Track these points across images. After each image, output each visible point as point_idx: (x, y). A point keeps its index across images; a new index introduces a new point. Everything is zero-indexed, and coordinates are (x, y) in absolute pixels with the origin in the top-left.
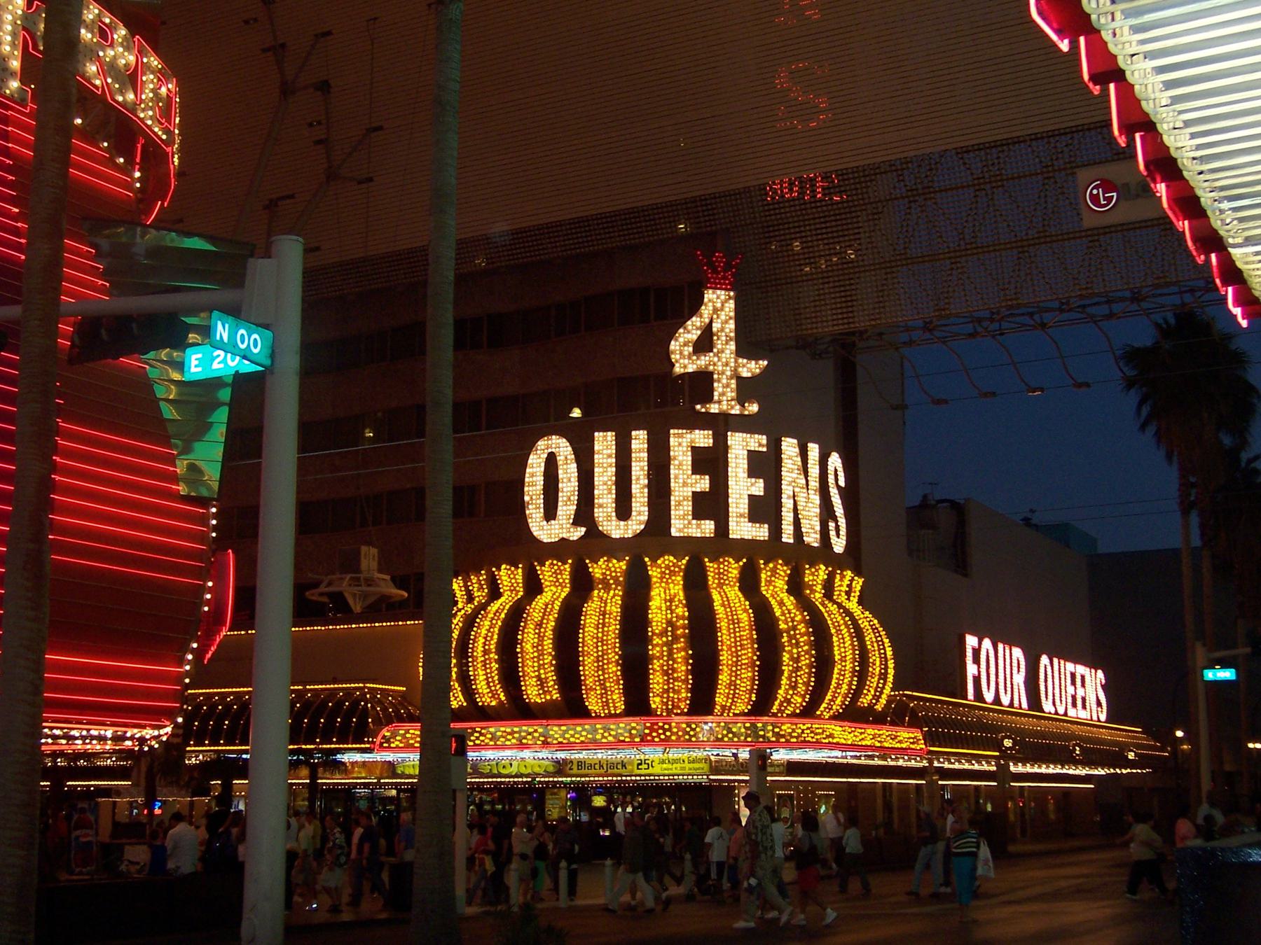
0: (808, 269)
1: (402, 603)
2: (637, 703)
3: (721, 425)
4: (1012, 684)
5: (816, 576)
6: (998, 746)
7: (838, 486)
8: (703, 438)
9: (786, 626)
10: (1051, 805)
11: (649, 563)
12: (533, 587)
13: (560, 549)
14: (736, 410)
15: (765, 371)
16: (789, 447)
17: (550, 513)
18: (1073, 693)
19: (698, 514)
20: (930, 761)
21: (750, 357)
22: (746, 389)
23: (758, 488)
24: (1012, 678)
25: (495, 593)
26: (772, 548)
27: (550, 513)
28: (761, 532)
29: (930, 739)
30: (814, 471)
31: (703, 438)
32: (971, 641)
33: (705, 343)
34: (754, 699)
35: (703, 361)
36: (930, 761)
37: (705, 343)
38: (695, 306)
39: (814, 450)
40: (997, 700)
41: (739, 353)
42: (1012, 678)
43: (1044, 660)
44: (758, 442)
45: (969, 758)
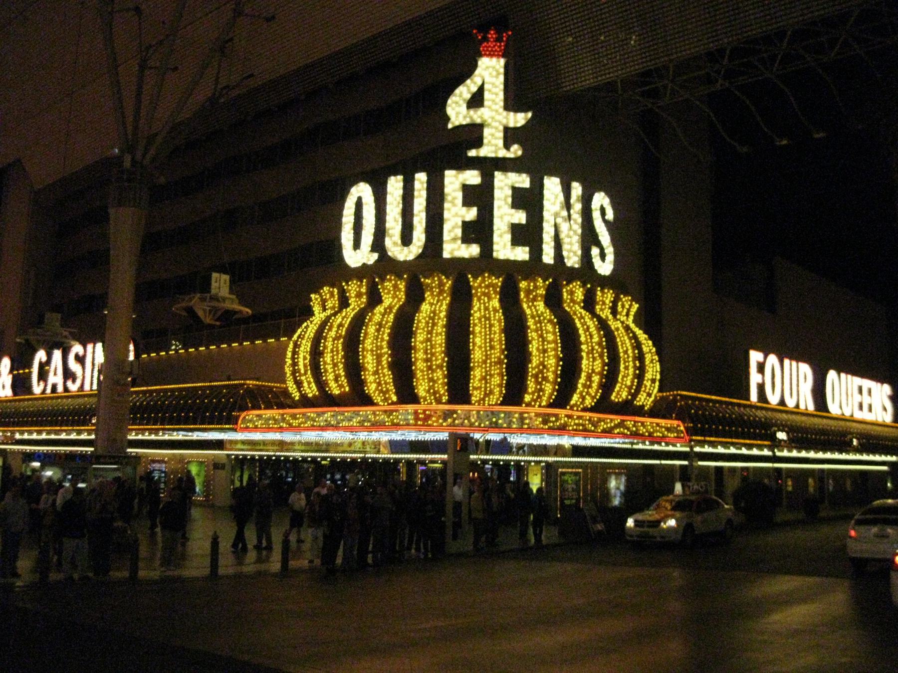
0: (570, 39)
1: (246, 320)
2: (407, 394)
3: (488, 167)
4: (798, 391)
5: (575, 292)
6: (773, 438)
7: (606, 222)
8: (473, 177)
9: (535, 327)
10: (848, 483)
11: (471, 279)
12: (374, 299)
13: (363, 272)
14: (502, 153)
15: (529, 122)
16: (552, 186)
17: (357, 245)
18: (760, 381)
19: (466, 239)
20: (691, 448)
21: (517, 110)
22: (510, 136)
23: (520, 217)
24: (798, 386)
25: (344, 302)
26: (534, 267)
27: (357, 245)
28: (522, 254)
29: (690, 432)
30: (577, 207)
31: (473, 177)
32: (755, 356)
33: (476, 101)
34: (504, 392)
35: (477, 116)
36: (691, 448)
37: (476, 101)
38: (469, 70)
39: (577, 189)
40: (782, 402)
41: (508, 107)
42: (798, 386)
43: (832, 375)
44: (523, 181)
45: (750, 447)
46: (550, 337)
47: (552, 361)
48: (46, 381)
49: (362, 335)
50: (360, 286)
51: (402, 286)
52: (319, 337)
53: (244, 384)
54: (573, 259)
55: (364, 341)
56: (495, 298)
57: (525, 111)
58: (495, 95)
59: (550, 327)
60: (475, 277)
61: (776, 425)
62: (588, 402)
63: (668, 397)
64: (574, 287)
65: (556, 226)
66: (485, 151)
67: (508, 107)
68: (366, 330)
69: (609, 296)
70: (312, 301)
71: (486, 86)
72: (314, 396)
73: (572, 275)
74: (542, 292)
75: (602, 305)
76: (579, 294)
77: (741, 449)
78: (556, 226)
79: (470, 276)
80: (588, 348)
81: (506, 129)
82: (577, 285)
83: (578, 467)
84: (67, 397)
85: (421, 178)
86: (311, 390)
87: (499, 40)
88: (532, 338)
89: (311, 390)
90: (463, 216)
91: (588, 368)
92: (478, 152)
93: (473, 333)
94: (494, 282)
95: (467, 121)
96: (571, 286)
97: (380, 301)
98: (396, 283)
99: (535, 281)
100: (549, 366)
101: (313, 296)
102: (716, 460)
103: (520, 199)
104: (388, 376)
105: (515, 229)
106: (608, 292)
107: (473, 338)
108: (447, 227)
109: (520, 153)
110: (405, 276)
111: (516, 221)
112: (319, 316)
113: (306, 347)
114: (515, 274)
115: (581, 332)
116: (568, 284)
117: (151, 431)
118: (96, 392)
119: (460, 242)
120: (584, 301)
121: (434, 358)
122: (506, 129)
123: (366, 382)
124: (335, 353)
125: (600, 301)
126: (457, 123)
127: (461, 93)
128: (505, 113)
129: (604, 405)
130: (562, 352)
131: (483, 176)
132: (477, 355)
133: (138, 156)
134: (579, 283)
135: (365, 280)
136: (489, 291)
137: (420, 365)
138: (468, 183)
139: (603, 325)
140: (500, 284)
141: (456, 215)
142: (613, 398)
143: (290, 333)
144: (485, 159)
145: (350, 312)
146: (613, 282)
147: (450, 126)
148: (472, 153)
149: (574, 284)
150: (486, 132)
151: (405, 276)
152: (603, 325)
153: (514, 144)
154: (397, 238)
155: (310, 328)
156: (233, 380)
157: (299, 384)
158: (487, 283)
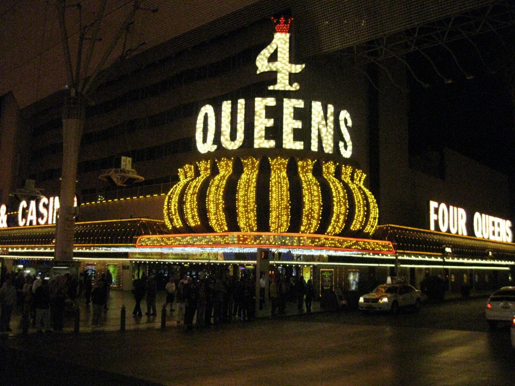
0: (327, 22)
1: (141, 184)
2: (233, 226)
3: (280, 96)
4: (458, 225)
5: (330, 168)
6: (443, 251)
7: (347, 127)
8: (271, 102)
9: (307, 188)
10: (487, 277)
11: (270, 160)
12: (215, 171)
13: (208, 156)
14: (288, 88)
15: (303, 70)
16: (317, 107)
17: (205, 141)
18: (436, 219)
19: (268, 137)
20: (397, 257)
21: (296, 63)
22: (293, 78)
23: (298, 124)
24: (458, 221)
25: (197, 173)
26: (306, 153)
27: (205, 141)
28: (299, 146)
29: (396, 248)
30: (331, 119)
31: (271, 102)
32: (433, 204)
33: (273, 58)
34: (289, 225)
35: (274, 66)
36: (397, 257)
37: (273, 58)
38: (269, 40)
39: (331, 108)
40: (449, 231)
41: (291, 61)
42: (458, 221)
43: (477, 215)
44: (300, 104)
45: (430, 256)
46: (316, 193)
47: (317, 207)
48: (26, 219)
49: (208, 192)
50: (207, 164)
51: (231, 164)
52: (183, 193)
53: (140, 220)
54: (328, 149)
55: (209, 195)
56: (284, 171)
57: (301, 63)
58: (284, 54)
59: (315, 188)
60: (273, 159)
61: (445, 244)
62: (337, 230)
63: (383, 228)
64: (329, 164)
65: (319, 130)
66: (278, 87)
67: (291, 61)
68: (210, 189)
69: (349, 170)
70: (179, 172)
71: (279, 50)
72: (180, 227)
73: (328, 158)
74: (311, 167)
75: (345, 175)
76: (332, 169)
77: (425, 258)
78: (319, 130)
79: (269, 158)
80: (337, 199)
81: (290, 74)
82: (331, 163)
83: (331, 268)
84: (39, 228)
85: (241, 102)
86: (178, 224)
87: (286, 23)
88: (305, 194)
89: (178, 224)
90: (266, 124)
91: (337, 211)
92: (274, 87)
93: (271, 191)
94: (283, 161)
95: (268, 69)
96: (328, 164)
97: (218, 173)
98: (227, 162)
99: (307, 161)
100: (315, 210)
101: (179, 170)
102: (410, 264)
103: (298, 114)
104: (222, 216)
105: (295, 131)
106: (349, 167)
107: (271, 194)
108: (256, 130)
109: (298, 88)
110: (232, 158)
111: (296, 127)
112: (183, 181)
113: (175, 199)
114: (296, 157)
115: (333, 190)
116: (325, 163)
117: (87, 247)
118: (55, 225)
119: (264, 139)
120: (335, 173)
121: (249, 206)
122: (290, 74)
123: (210, 219)
124: (192, 203)
125: (344, 172)
126: (262, 71)
127: (264, 53)
128: (290, 65)
129: (346, 232)
130: (322, 202)
131: (277, 101)
132: (274, 204)
133: (79, 90)
134: (332, 162)
135: (209, 161)
136: (281, 167)
137: (241, 209)
138: (268, 105)
139: (346, 186)
140: (286, 163)
141: (262, 123)
142: (351, 228)
143: (166, 191)
144: (278, 91)
145: (201, 179)
146: (352, 162)
147: (258, 72)
148: (271, 88)
149: (329, 163)
150: (279, 76)
151: (232, 158)
152: (346, 186)
153: (295, 82)
154: (228, 136)
155: (178, 188)
156: (134, 218)
157: (171, 220)
158: (279, 162)
